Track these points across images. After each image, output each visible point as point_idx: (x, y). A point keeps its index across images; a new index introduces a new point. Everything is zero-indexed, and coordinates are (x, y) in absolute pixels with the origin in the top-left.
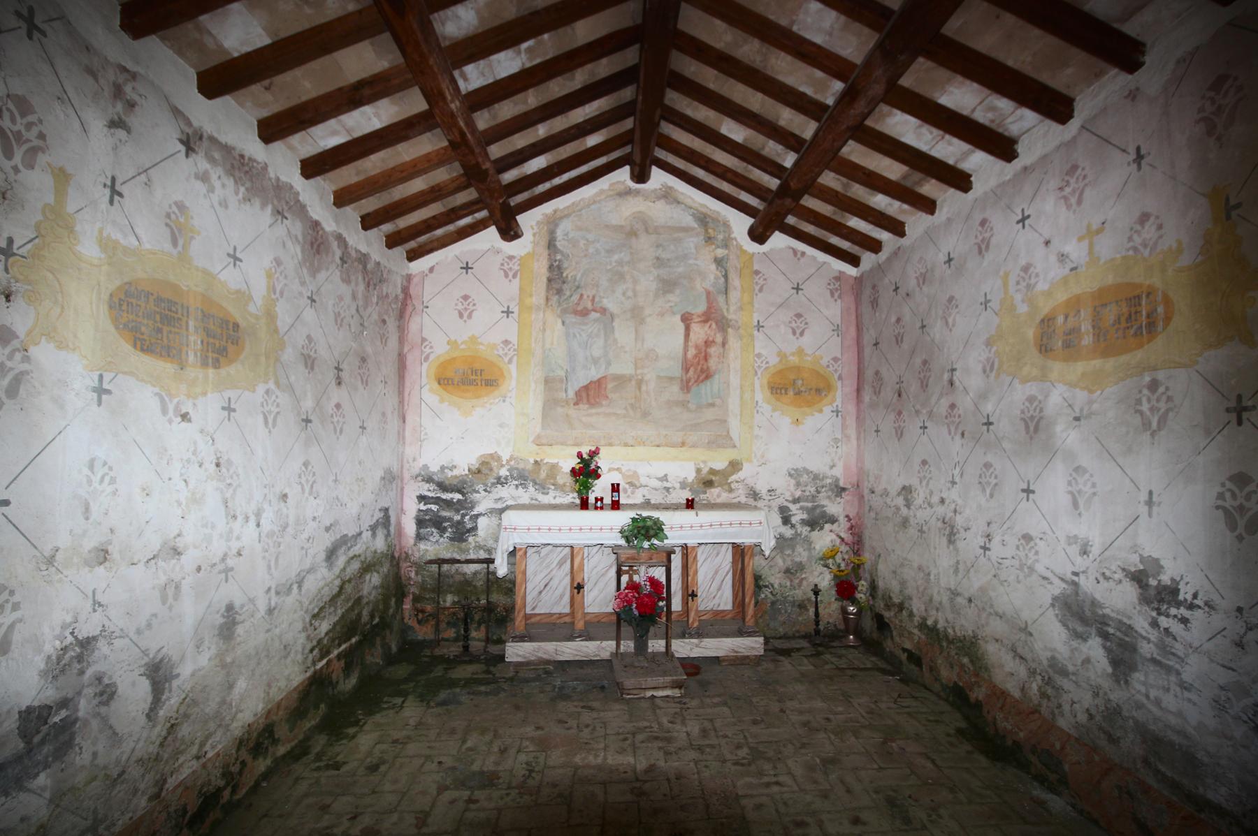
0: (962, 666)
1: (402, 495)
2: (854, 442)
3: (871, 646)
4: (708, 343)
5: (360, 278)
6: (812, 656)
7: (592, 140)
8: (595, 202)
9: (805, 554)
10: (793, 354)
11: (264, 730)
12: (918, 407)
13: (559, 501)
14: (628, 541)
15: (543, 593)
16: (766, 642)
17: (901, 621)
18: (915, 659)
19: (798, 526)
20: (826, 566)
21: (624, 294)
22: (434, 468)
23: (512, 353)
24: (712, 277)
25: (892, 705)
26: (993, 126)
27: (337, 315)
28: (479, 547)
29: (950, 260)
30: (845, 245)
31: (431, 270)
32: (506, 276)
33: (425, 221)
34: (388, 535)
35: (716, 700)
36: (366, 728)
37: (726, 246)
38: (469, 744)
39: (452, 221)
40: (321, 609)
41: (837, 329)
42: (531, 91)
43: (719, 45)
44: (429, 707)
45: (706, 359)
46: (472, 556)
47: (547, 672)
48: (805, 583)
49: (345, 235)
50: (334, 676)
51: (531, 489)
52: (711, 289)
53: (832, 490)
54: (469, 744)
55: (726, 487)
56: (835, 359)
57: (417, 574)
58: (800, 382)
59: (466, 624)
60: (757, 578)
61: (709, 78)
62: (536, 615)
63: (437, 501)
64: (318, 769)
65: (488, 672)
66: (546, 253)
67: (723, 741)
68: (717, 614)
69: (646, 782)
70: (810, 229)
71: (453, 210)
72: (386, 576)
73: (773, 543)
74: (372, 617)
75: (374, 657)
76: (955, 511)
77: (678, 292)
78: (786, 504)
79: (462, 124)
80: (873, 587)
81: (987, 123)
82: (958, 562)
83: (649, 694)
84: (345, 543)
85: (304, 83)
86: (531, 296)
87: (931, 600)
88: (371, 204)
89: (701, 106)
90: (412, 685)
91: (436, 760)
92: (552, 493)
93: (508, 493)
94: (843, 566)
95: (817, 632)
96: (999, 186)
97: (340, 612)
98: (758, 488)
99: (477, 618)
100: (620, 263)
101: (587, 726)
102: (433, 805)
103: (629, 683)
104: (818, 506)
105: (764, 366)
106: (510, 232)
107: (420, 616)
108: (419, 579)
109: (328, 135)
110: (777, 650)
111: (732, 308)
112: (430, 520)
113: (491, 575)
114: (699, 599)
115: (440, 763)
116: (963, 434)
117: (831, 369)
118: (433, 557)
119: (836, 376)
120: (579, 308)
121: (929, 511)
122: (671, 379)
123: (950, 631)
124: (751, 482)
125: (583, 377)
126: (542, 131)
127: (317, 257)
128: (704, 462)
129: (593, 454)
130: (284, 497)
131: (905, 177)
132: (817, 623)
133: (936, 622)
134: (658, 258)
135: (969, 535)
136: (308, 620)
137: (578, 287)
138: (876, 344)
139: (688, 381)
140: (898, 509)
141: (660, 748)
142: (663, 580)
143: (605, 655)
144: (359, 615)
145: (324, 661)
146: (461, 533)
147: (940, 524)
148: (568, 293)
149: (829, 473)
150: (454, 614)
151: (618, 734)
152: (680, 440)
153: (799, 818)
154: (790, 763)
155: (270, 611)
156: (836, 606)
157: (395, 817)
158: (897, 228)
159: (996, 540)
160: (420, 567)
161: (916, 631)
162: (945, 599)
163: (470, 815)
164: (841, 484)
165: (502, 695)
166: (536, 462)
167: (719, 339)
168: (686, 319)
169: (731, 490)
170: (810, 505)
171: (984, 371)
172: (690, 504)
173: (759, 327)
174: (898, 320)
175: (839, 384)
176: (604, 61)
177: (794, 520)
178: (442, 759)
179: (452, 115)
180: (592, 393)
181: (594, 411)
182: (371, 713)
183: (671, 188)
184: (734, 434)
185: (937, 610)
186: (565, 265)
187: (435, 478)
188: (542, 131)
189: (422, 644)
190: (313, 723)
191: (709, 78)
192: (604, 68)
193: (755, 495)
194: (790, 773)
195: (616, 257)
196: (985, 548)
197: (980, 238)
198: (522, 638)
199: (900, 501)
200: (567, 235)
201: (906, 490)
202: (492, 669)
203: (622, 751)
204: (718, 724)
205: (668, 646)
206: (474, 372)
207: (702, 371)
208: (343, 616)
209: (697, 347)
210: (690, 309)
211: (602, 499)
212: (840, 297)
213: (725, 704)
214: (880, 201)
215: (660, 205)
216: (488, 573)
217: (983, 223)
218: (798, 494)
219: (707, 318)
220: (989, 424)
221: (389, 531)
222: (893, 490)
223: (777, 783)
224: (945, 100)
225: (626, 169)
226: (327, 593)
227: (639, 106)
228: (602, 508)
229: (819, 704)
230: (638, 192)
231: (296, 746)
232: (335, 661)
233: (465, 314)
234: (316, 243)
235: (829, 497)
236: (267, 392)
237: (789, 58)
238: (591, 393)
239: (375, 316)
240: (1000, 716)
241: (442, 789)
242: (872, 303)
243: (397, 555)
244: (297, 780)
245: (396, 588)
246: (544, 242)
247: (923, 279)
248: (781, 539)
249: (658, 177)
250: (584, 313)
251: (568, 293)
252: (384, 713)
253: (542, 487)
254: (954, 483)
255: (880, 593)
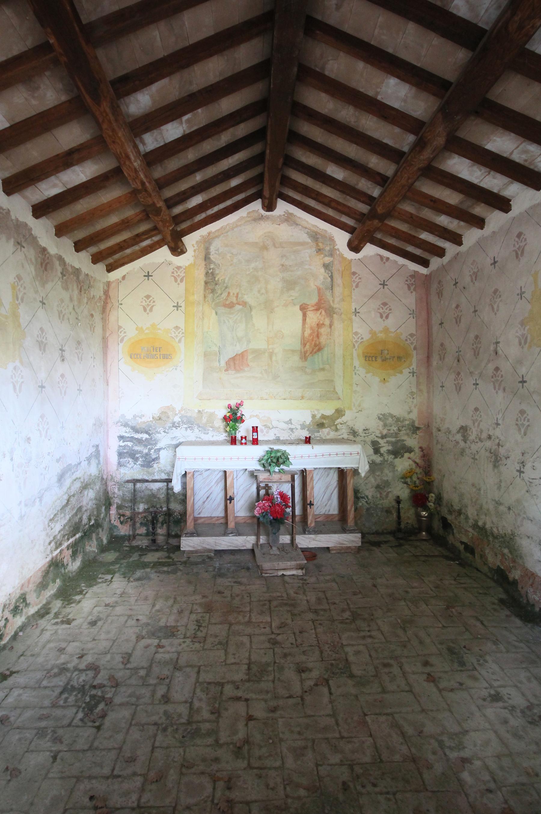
0: (503, 555)
1: (108, 435)
2: (425, 394)
3: (439, 540)
4: (319, 326)
5: (75, 287)
6: (396, 546)
7: (235, 182)
8: (237, 226)
9: (390, 474)
10: (381, 332)
11: (20, 597)
12: (472, 369)
13: (215, 439)
14: (264, 466)
15: (206, 502)
16: (363, 537)
17: (460, 522)
18: (470, 549)
19: (385, 455)
20: (406, 483)
21: (259, 291)
22: (129, 416)
23: (181, 335)
24: (322, 277)
25: (453, 582)
26: (526, 164)
27: (60, 313)
28: (162, 471)
29: (495, 262)
30: (418, 252)
31: (124, 278)
32: (176, 280)
33: (118, 244)
34: (99, 463)
35: (328, 578)
36: (87, 595)
37: (331, 255)
38: (157, 607)
39: (137, 243)
40: (55, 515)
41: (412, 313)
42: (190, 149)
43: (325, 111)
44: (129, 581)
45: (318, 336)
46: (157, 477)
47: (210, 558)
48: (390, 495)
49: (64, 256)
50: (65, 560)
51: (196, 430)
52: (321, 286)
53: (410, 429)
54: (157, 607)
55: (333, 428)
56: (412, 335)
57: (119, 490)
58: (386, 352)
59: (153, 524)
60: (356, 492)
61: (316, 134)
62: (201, 518)
63: (132, 439)
64: (56, 623)
65: (169, 557)
66: (203, 263)
67: (332, 607)
68: (328, 517)
69: (279, 634)
70: (392, 241)
71: (137, 235)
72: (99, 492)
73: (367, 467)
74: (90, 520)
75: (92, 547)
76: (499, 445)
77: (297, 289)
78: (376, 439)
79: (142, 176)
80: (439, 499)
81: (522, 162)
82: (501, 481)
83: (280, 573)
84: (70, 470)
85: (34, 152)
86: (193, 294)
87: (481, 508)
88: (81, 234)
89: (311, 155)
90: (118, 566)
91: (135, 618)
92: (211, 433)
93: (181, 434)
94: (417, 482)
95: (399, 530)
96: (531, 208)
97: (68, 517)
98: (356, 428)
99: (161, 519)
100: (256, 269)
101: (238, 596)
102: (134, 649)
103: (266, 565)
104: (400, 440)
105: (360, 341)
106: (177, 249)
107: (122, 519)
108: (121, 493)
109: (50, 188)
110: (371, 541)
111: (337, 300)
112: (127, 453)
113: (169, 489)
114: (315, 507)
115: (138, 620)
116: (504, 390)
117: (409, 342)
118: (130, 478)
119: (412, 347)
120: (227, 303)
121: (480, 444)
122: (293, 351)
123: (495, 530)
124: (350, 424)
125: (230, 352)
126: (199, 177)
127: (45, 273)
128: (318, 410)
129: (239, 406)
130: (29, 439)
131: (461, 202)
132: (399, 523)
133: (485, 524)
134: (283, 265)
135: (509, 462)
136: (46, 523)
137: (226, 287)
138: (441, 324)
139: (305, 353)
140: (458, 443)
141: (288, 611)
142: (289, 494)
143: (249, 546)
144: (81, 519)
145: (58, 550)
146: (149, 462)
147: (488, 454)
148: (219, 292)
149: (407, 417)
150: (145, 517)
151: (259, 601)
152: (300, 395)
153: (386, 661)
154: (380, 622)
155: (22, 517)
156: (412, 511)
157: (108, 657)
158: (457, 239)
159: (529, 465)
160: (121, 485)
161: (470, 530)
162: (491, 507)
163: (158, 656)
164: (417, 425)
165: (179, 573)
166: (199, 411)
167: (327, 322)
168: (303, 308)
169: (337, 430)
170: (393, 440)
171: (520, 344)
172: (308, 441)
173: (356, 312)
174: (457, 306)
175: (415, 352)
176: (242, 126)
177: (382, 450)
178: (140, 617)
179: (136, 171)
180: (237, 362)
181: (239, 375)
182: (91, 586)
183: (291, 214)
184: (339, 389)
185: (486, 515)
186: (217, 272)
187: (130, 423)
188: (199, 177)
189: (123, 538)
190: (52, 592)
191: (316, 134)
192: (241, 130)
193: (354, 433)
194: (379, 629)
195: (253, 265)
196: (520, 472)
197: (517, 246)
198: (192, 535)
199: (459, 437)
200: (218, 250)
201: (464, 430)
202: (171, 555)
203: (262, 613)
204: (329, 594)
205: (293, 540)
206: (155, 349)
207: (315, 345)
208: (70, 520)
209: (311, 328)
210: (307, 301)
211: (245, 438)
212: (415, 290)
213: (334, 580)
214: (443, 220)
215: (284, 227)
216: (168, 489)
217: (519, 235)
218: (385, 432)
219: (318, 307)
220: (523, 382)
221: (99, 461)
222: (454, 429)
223: (370, 637)
224: (489, 147)
225: (259, 201)
226: (59, 504)
227: (267, 157)
228: (246, 444)
229: (401, 581)
230: (268, 218)
231: (41, 608)
232: (66, 550)
233: (147, 309)
234: (45, 262)
235: (408, 434)
236: (15, 368)
237: (375, 119)
238: (237, 362)
239: (86, 312)
240: (530, 590)
241: (140, 638)
242: (438, 294)
243: (105, 477)
244: (43, 630)
245: (106, 501)
246: (202, 256)
247: (475, 276)
248: (373, 465)
249: (282, 207)
250: (231, 306)
251: (219, 292)
252: (101, 585)
253: (204, 429)
254: (497, 424)
255: (444, 502)
